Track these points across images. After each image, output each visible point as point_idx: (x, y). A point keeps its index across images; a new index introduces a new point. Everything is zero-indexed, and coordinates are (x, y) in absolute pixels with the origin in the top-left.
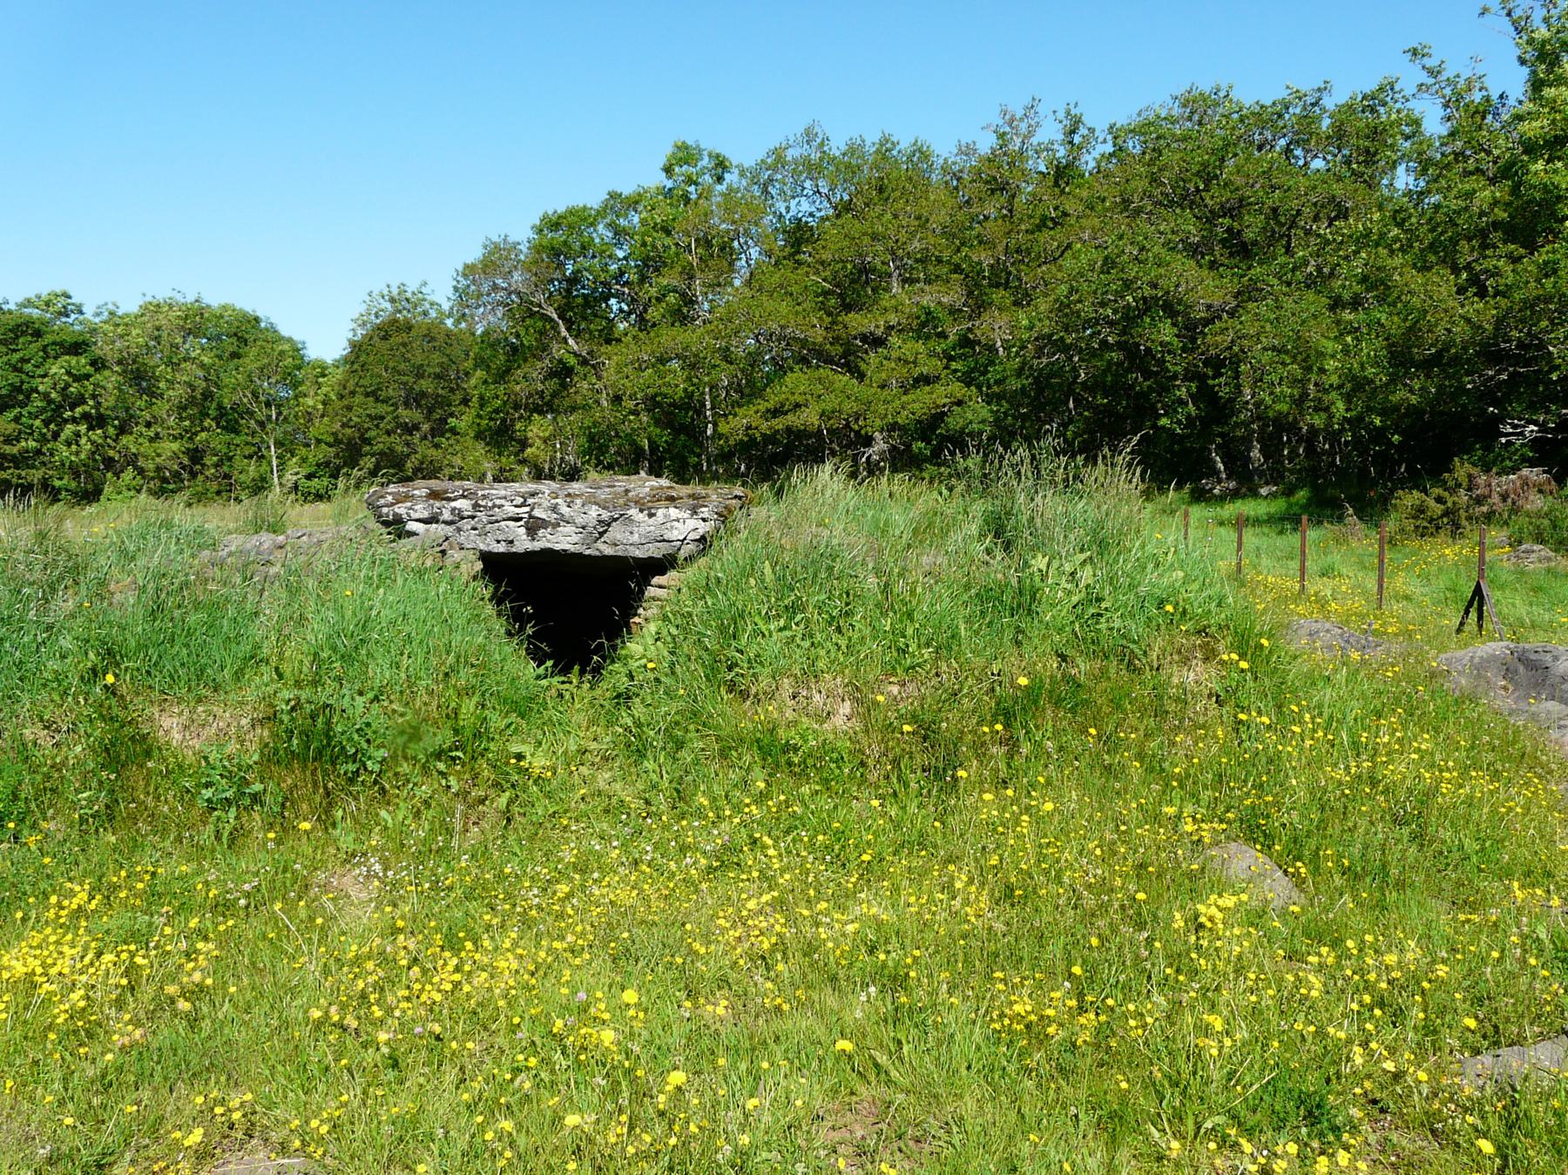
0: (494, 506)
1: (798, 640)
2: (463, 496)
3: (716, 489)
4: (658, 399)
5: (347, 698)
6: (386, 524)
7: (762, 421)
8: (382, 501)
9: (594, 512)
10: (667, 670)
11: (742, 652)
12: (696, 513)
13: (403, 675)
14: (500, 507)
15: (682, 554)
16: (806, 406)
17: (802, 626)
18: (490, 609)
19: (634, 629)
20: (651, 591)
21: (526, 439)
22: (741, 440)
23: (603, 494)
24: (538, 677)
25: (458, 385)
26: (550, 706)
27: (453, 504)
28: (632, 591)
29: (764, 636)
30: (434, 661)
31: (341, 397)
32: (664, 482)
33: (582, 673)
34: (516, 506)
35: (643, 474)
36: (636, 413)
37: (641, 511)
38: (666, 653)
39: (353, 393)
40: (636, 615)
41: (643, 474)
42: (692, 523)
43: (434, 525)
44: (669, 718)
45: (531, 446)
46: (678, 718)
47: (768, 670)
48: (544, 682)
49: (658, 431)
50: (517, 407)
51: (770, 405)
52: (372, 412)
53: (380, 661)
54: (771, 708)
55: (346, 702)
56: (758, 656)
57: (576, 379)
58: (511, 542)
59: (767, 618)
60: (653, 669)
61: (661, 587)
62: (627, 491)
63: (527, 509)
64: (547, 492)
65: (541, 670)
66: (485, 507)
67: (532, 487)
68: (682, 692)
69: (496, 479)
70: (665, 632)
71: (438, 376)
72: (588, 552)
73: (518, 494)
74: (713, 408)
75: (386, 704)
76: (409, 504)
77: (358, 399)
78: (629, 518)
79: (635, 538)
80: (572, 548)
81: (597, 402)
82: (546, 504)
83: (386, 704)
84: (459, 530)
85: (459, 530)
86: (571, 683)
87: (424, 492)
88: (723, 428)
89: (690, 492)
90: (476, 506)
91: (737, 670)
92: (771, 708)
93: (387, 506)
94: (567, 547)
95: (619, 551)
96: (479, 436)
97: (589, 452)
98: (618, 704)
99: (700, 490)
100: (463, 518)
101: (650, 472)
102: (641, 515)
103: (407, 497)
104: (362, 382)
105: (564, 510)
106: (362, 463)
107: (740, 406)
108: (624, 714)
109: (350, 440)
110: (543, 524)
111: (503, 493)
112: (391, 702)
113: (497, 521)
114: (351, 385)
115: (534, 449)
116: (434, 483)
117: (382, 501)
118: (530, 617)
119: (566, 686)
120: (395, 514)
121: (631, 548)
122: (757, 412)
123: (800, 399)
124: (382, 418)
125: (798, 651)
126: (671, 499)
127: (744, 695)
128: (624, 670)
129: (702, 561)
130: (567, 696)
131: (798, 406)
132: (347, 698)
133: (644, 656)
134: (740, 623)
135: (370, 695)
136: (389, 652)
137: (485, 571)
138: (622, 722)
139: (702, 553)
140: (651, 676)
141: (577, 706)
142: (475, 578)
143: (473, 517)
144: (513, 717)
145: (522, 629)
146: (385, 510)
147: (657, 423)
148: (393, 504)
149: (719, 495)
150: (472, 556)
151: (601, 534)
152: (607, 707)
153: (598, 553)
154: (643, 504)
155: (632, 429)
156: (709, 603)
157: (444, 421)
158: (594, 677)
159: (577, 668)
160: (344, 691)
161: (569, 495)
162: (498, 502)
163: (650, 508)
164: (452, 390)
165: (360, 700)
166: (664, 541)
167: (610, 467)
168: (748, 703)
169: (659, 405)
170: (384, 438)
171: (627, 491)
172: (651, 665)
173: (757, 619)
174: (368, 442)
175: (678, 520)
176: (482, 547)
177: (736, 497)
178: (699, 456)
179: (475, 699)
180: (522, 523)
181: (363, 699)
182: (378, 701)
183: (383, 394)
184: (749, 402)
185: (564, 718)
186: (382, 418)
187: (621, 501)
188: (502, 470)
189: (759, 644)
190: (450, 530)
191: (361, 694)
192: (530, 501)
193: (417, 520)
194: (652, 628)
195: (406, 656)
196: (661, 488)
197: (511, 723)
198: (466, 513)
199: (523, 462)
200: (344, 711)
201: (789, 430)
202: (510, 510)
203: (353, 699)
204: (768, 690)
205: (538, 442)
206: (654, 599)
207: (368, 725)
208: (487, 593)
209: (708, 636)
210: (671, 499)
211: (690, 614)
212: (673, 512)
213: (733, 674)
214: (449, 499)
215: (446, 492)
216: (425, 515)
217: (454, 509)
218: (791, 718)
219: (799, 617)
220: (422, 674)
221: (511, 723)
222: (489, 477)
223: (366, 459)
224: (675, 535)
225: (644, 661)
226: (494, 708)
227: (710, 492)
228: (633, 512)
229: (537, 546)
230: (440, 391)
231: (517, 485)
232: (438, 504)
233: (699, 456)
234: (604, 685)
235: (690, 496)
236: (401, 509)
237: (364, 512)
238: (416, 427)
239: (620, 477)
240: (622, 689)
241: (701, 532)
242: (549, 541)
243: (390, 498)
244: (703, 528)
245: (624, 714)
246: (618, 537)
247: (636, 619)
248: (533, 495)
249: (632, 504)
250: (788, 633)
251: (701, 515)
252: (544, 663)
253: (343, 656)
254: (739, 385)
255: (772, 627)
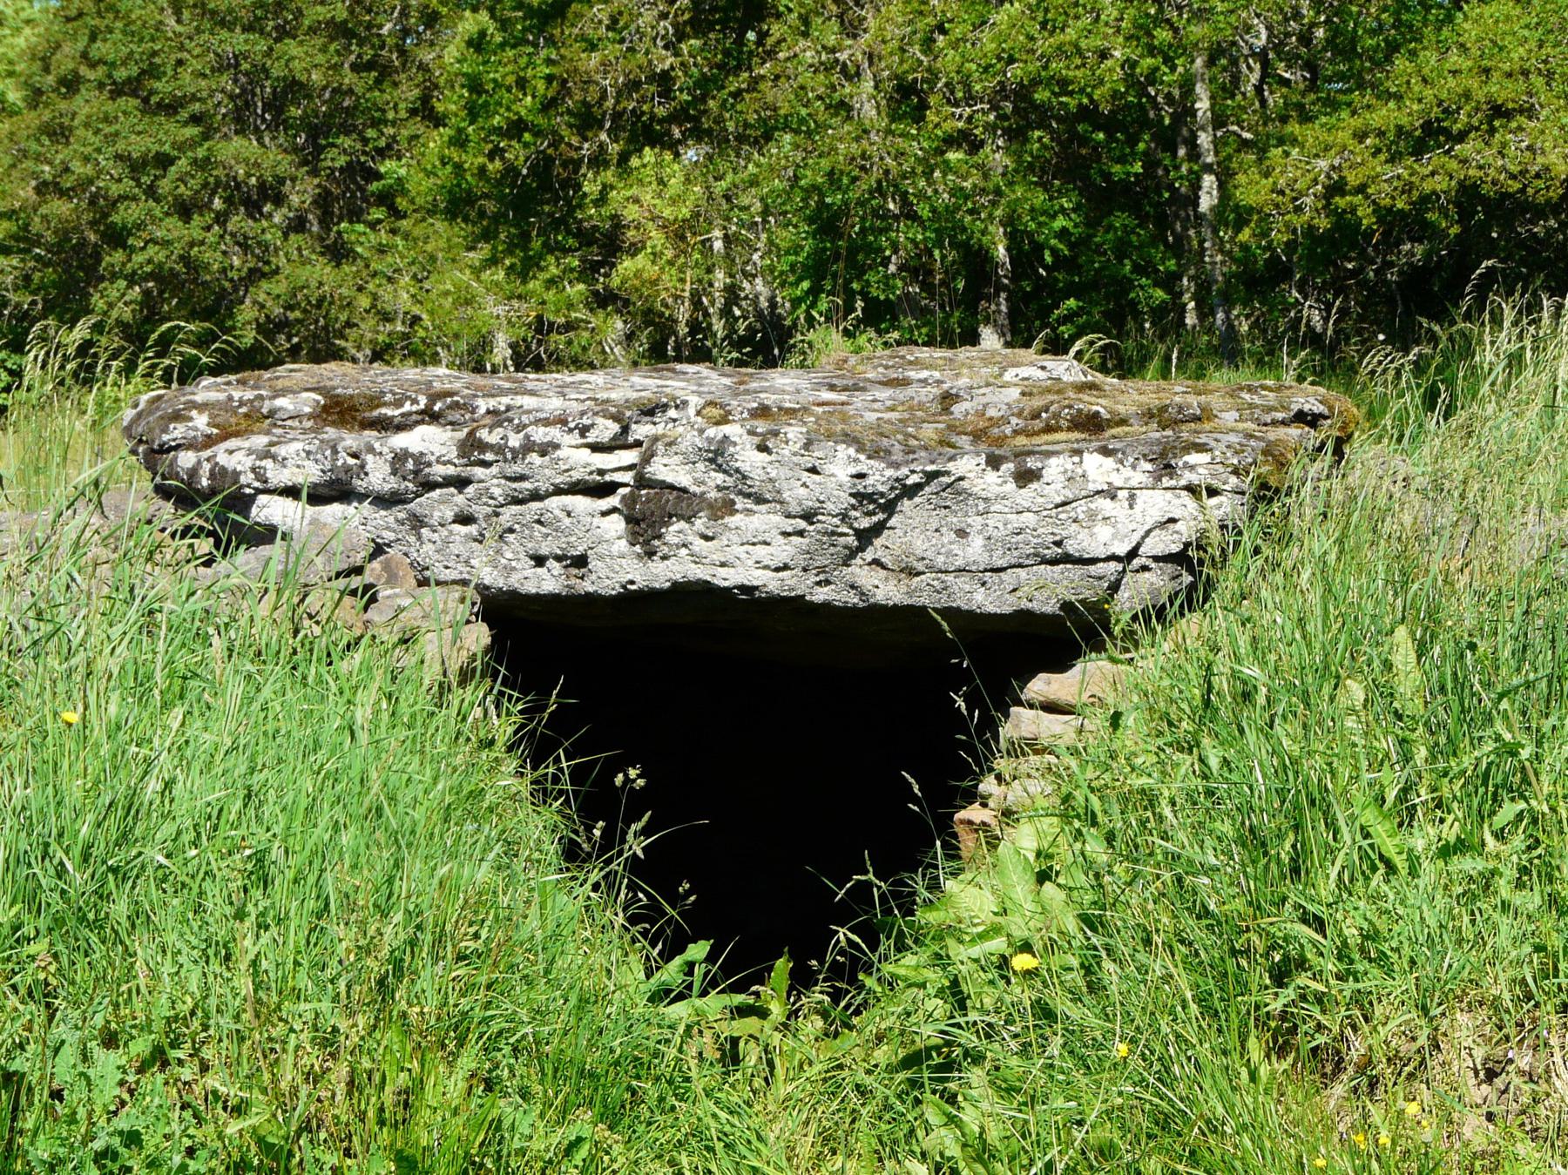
0: (528, 447)
1: (1504, 888)
2: (429, 416)
3: (1233, 394)
4: (1041, 95)
5: (69, 1055)
6: (184, 496)
7: (1378, 166)
8: (178, 432)
9: (841, 465)
10: (1077, 978)
11: (1319, 924)
12: (1169, 469)
13: (245, 985)
14: (545, 449)
15: (1126, 602)
16: (1530, 112)
17: (1518, 841)
18: (510, 779)
19: (967, 842)
20: (1021, 723)
21: (617, 223)
22: (1310, 229)
23: (870, 408)
24: (663, 995)
25: (403, 52)
26: (698, 1086)
27: (400, 441)
28: (960, 722)
29: (1391, 868)
30: (343, 938)
31: (36, 97)
32: (1066, 369)
33: (801, 980)
34: (596, 448)
35: (990, 339)
36: (967, 140)
37: (994, 462)
38: (1072, 925)
39: (71, 84)
40: (971, 796)
41: (990, 339)
42: (1157, 503)
43: (336, 508)
44: (1078, 1135)
45: (634, 250)
46: (1110, 1133)
47: (1402, 984)
48: (680, 1011)
49: (1040, 198)
50: (587, 121)
51: (1407, 115)
52: (138, 146)
53: (171, 938)
54: (1412, 1109)
55: (64, 1068)
56: (1372, 935)
57: (776, 30)
58: (581, 561)
59: (1406, 816)
60: (1029, 974)
61: (1051, 708)
62: (948, 399)
63: (629, 457)
64: (695, 401)
65: (672, 972)
66: (499, 449)
67: (644, 384)
68: (1123, 1049)
69: (527, 359)
70: (1065, 852)
71: (340, 31)
72: (821, 595)
73: (604, 408)
74: (1219, 121)
75: (187, 1074)
76: (260, 441)
77: (86, 104)
78: (956, 488)
79: (974, 551)
80: (771, 583)
81: (843, 108)
82: (690, 440)
83: (187, 1074)
84: (417, 522)
85: (417, 522)
86: (763, 1014)
87: (308, 401)
88: (1252, 190)
89: (1152, 400)
90: (471, 447)
91: (1303, 979)
92: (1412, 1109)
93: (191, 445)
94: (757, 577)
95: (922, 593)
96: (457, 205)
97: (817, 270)
98: (914, 1084)
99: (1179, 392)
100: (429, 486)
101: (1019, 336)
102: (992, 476)
103: (257, 418)
104: (100, 49)
105: (749, 459)
106: (98, 302)
107: (1306, 118)
108: (933, 1117)
109: (64, 235)
110: (680, 503)
111: (554, 404)
112: (205, 1068)
113: (536, 496)
114: (65, 61)
115: (641, 260)
116: (335, 374)
117: (178, 432)
118: (637, 804)
119: (751, 1024)
120: (219, 473)
121: (961, 584)
122: (1360, 136)
123: (1502, 91)
124: (164, 161)
125: (1504, 922)
126: (1091, 424)
127: (1328, 1062)
128: (936, 978)
129: (1192, 625)
130: (751, 1056)
131: (1498, 111)
132: (69, 1055)
133: (995, 930)
134: (1317, 833)
135: (141, 1046)
136: (199, 909)
137: (496, 649)
138: (928, 1143)
139: (1195, 597)
140: (1022, 994)
141: (782, 1089)
142: (465, 676)
143: (461, 483)
144: (583, 1124)
145: (612, 840)
146: (186, 459)
147: (1041, 172)
148: (210, 441)
149: (1247, 411)
150: (453, 605)
151: (866, 537)
152: (881, 1092)
153: (853, 599)
154: (1000, 441)
155: (956, 191)
156: (1214, 763)
157: (360, 172)
158: (836, 996)
159: (782, 966)
160: (60, 1031)
161: (763, 412)
162: (540, 434)
163: (1020, 455)
164: (384, 73)
165: (108, 1063)
166: (1067, 559)
167: (879, 315)
168: (1339, 1089)
169: (1042, 116)
170: (172, 228)
171: (948, 399)
172: (1022, 962)
173: (1369, 817)
174: (117, 238)
175: (1111, 493)
176: (492, 578)
177: (1301, 418)
178: (1169, 282)
179: (468, 1061)
180: (613, 501)
181: (114, 1058)
182: (165, 1064)
183: (162, 87)
184: (1332, 105)
185: (740, 1127)
186: (164, 161)
187: (929, 432)
188: (542, 327)
189: (1375, 898)
190: (384, 522)
191: (110, 1040)
192: (641, 431)
193: (292, 492)
194: (1025, 839)
195: (250, 921)
196: (1057, 386)
197: (579, 1140)
198: (439, 471)
199: (604, 300)
200: (57, 1095)
201: (1468, 194)
202: (579, 460)
203: (85, 1057)
204: (1406, 1048)
205: (657, 238)
206: (1033, 746)
207: (132, 1139)
208: (504, 728)
209: (1210, 871)
210: (1091, 424)
211: (1149, 799)
212: (1098, 469)
213: (1289, 993)
214: (385, 426)
215: (375, 401)
216: (310, 473)
217: (400, 457)
218: (1479, 1143)
219: (1508, 811)
220: (303, 981)
221: (579, 1140)
222: (501, 351)
223: (115, 289)
224: (1102, 540)
225: (998, 945)
226: (525, 1094)
227: (1215, 401)
228: (968, 465)
229: (660, 574)
230: (349, 78)
231: (598, 378)
232: (351, 440)
233: (1169, 282)
234: (872, 1023)
235: (1149, 415)
236: (236, 457)
237: (121, 461)
238: (272, 193)
239: (924, 353)
240: (928, 1034)
241: (1185, 530)
242: (697, 559)
243: (201, 421)
244: (1190, 520)
245: (933, 1117)
246: (920, 545)
247: (974, 813)
248: (650, 411)
249: (964, 441)
250: (1469, 864)
251: (1188, 477)
252: (681, 950)
253: (59, 921)
254: (1305, 39)
255: (1419, 844)
